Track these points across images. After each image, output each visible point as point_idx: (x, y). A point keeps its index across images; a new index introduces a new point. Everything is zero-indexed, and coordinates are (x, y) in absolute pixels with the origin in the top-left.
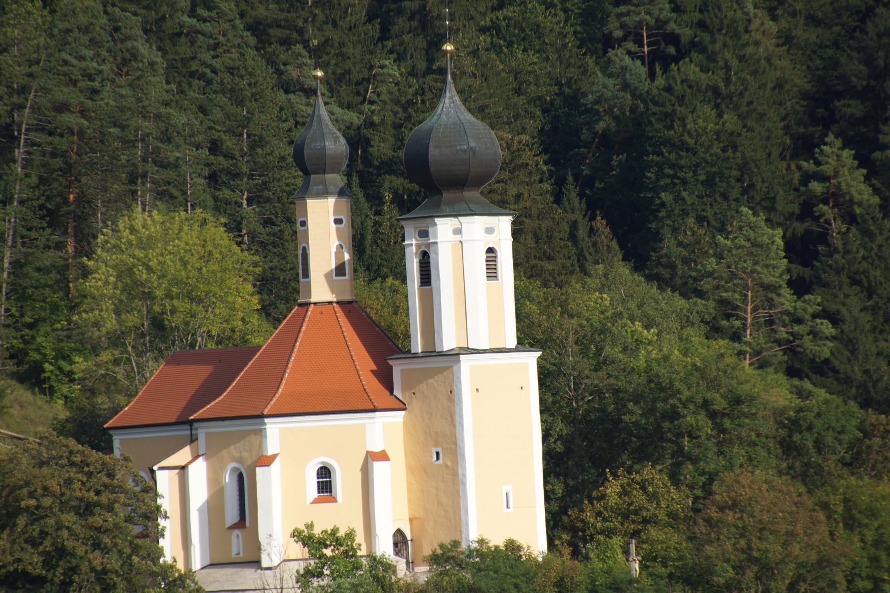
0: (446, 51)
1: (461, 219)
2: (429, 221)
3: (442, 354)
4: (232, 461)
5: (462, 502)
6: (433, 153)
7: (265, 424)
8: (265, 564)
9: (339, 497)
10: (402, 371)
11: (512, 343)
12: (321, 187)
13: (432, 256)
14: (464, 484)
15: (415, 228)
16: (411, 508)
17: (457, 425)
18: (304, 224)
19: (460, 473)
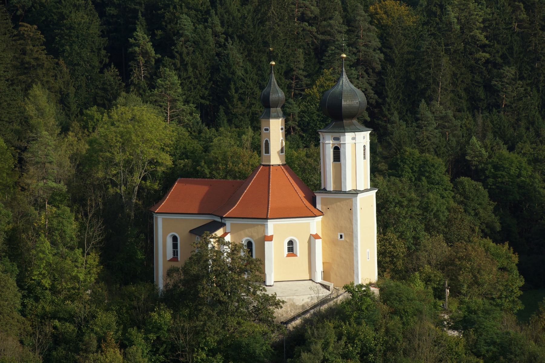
0: (342, 57)
2: (341, 134)
3: (345, 193)
8: (268, 284)
9: (298, 255)
10: (322, 198)
11: (369, 188)
12: (275, 114)
13: (342, 150)
14: (357, 250)
15: (332, 136)
16: (323, 258)
17: (354, 224)
19: (354, 244)
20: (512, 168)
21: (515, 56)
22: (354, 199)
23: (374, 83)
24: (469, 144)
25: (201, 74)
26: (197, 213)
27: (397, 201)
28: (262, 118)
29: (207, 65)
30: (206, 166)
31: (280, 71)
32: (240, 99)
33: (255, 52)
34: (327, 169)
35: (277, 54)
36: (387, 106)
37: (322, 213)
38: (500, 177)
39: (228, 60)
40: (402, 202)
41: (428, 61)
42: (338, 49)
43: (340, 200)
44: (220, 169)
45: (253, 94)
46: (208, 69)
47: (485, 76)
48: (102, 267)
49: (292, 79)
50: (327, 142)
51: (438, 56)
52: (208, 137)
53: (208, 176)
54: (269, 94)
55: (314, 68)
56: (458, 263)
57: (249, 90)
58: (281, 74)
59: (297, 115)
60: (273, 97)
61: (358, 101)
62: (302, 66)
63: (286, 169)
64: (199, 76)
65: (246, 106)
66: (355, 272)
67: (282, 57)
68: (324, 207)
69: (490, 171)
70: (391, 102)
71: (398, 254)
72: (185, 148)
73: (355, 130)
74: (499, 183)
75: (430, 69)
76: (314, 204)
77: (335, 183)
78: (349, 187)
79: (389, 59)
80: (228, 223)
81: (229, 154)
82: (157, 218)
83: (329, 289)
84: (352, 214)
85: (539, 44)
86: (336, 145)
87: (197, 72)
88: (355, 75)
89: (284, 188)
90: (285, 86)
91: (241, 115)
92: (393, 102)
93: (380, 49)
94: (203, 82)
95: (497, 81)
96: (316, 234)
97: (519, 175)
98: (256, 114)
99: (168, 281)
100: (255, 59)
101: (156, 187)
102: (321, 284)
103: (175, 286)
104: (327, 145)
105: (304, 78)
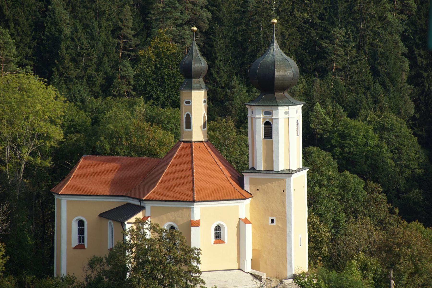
0: (273, 23)
1: (290, 107)
2: (273, 107)
3: (277, 172)
4: (169, 221)
5: (288, 244)
6: (277, 74)
7: (194, 205)
9: (226, 241)
10: (250, 178)
11: (301, 167)
12: (198, 85)
13: (274, 126)
14: (290, 237)
15: (263, 110)
17: (287, 207)
18: (188, 103)
19: (288, 230)
20: (360, 137)
21: (340, 16)
22: (287, 180)
23: (202, 44)
24: (312, 111)
25: (23, 31)
26: (108, 194)
27: (316, 180)
28: (183, 90)
29: (30, 21)
30: (106, 141)
31: (107, 29)
32: (74, 60)
33: (79, 7)
34: (257, 146)
35: (105, 11)
36: (216, 69)
37: (251, 195)
38: (347, 147)
39: (54, 16)
40: (321, 181)
41: (257, 21)
42: (169, 6)
43: (271, 181)
44: (123, 145)
45: (88, 55)
46: (31, 26)
47: (313, 37)
48: (8, 257)
49: (120, 39)
50: (257, 117)
51: (268, 16)
52: (94, 107)
53: (108, 152)
54: (191, 63)
55: (139, 27)
56: (397, 250)
57: (85, 51)
58: (108, 33)
59: (132, 79)
60: (196, 66)
61: (291, 72)
62: (130, 25)
63: (209, 146)
64: (21, 33)
65: (81, 68)
66: (288, 261)
67: (109, 14)
68: (253, 188)
69: (337, 140)
70: (220, 65)
71: (322, 239)
72: (73, 121)
73: (288, 104)
74: (346, 153)
75: (260, 29)
76: (242, 185)
77: (266, 161)
78: (281, 166)
79: (216, 19)
80: (148, 206)
81: (132, 128)
82: (59, 201)
83: (261, 280)
84: (285, 196)
85: (364, 3)
86: (268, 120)
87: (19, 28)
88: (188, 35)
89: (208, 168)
90: (113, 45)
91: (75, 78)
92: (222, 65)
93: (206, 7)
94: (27, 40)
95: (327, 43)
96: (246, 218)
97: (366, 144)
98: (92, 77)
99: (89, 272)
100: (80, 15)
101: (47, 164)
102: (251, 274)
103: (99, 280)
104: (257, 121)
105: (132, 38)
